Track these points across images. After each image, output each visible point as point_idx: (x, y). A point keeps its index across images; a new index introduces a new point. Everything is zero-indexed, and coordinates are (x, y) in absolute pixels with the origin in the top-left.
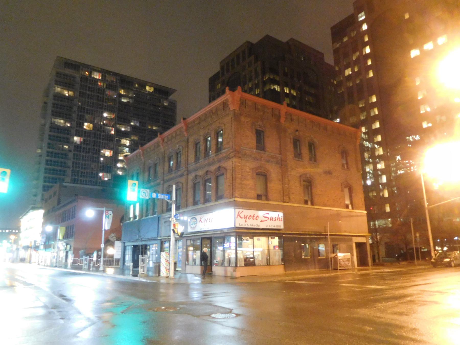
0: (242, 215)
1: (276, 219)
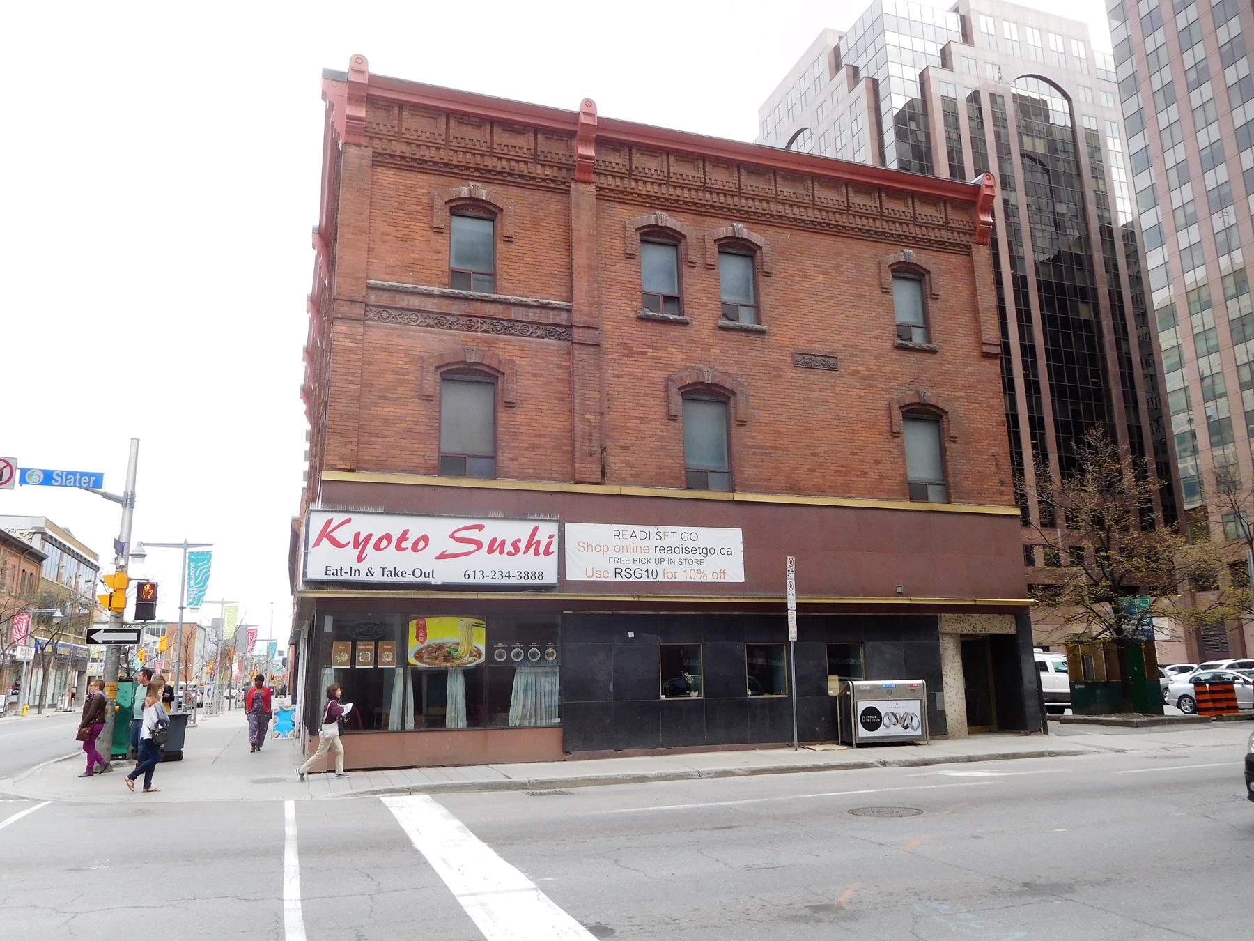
0: (344, 535)
1: (522, 546)
